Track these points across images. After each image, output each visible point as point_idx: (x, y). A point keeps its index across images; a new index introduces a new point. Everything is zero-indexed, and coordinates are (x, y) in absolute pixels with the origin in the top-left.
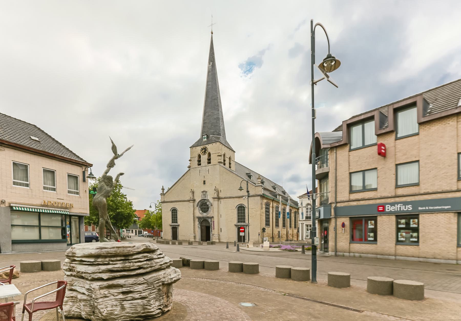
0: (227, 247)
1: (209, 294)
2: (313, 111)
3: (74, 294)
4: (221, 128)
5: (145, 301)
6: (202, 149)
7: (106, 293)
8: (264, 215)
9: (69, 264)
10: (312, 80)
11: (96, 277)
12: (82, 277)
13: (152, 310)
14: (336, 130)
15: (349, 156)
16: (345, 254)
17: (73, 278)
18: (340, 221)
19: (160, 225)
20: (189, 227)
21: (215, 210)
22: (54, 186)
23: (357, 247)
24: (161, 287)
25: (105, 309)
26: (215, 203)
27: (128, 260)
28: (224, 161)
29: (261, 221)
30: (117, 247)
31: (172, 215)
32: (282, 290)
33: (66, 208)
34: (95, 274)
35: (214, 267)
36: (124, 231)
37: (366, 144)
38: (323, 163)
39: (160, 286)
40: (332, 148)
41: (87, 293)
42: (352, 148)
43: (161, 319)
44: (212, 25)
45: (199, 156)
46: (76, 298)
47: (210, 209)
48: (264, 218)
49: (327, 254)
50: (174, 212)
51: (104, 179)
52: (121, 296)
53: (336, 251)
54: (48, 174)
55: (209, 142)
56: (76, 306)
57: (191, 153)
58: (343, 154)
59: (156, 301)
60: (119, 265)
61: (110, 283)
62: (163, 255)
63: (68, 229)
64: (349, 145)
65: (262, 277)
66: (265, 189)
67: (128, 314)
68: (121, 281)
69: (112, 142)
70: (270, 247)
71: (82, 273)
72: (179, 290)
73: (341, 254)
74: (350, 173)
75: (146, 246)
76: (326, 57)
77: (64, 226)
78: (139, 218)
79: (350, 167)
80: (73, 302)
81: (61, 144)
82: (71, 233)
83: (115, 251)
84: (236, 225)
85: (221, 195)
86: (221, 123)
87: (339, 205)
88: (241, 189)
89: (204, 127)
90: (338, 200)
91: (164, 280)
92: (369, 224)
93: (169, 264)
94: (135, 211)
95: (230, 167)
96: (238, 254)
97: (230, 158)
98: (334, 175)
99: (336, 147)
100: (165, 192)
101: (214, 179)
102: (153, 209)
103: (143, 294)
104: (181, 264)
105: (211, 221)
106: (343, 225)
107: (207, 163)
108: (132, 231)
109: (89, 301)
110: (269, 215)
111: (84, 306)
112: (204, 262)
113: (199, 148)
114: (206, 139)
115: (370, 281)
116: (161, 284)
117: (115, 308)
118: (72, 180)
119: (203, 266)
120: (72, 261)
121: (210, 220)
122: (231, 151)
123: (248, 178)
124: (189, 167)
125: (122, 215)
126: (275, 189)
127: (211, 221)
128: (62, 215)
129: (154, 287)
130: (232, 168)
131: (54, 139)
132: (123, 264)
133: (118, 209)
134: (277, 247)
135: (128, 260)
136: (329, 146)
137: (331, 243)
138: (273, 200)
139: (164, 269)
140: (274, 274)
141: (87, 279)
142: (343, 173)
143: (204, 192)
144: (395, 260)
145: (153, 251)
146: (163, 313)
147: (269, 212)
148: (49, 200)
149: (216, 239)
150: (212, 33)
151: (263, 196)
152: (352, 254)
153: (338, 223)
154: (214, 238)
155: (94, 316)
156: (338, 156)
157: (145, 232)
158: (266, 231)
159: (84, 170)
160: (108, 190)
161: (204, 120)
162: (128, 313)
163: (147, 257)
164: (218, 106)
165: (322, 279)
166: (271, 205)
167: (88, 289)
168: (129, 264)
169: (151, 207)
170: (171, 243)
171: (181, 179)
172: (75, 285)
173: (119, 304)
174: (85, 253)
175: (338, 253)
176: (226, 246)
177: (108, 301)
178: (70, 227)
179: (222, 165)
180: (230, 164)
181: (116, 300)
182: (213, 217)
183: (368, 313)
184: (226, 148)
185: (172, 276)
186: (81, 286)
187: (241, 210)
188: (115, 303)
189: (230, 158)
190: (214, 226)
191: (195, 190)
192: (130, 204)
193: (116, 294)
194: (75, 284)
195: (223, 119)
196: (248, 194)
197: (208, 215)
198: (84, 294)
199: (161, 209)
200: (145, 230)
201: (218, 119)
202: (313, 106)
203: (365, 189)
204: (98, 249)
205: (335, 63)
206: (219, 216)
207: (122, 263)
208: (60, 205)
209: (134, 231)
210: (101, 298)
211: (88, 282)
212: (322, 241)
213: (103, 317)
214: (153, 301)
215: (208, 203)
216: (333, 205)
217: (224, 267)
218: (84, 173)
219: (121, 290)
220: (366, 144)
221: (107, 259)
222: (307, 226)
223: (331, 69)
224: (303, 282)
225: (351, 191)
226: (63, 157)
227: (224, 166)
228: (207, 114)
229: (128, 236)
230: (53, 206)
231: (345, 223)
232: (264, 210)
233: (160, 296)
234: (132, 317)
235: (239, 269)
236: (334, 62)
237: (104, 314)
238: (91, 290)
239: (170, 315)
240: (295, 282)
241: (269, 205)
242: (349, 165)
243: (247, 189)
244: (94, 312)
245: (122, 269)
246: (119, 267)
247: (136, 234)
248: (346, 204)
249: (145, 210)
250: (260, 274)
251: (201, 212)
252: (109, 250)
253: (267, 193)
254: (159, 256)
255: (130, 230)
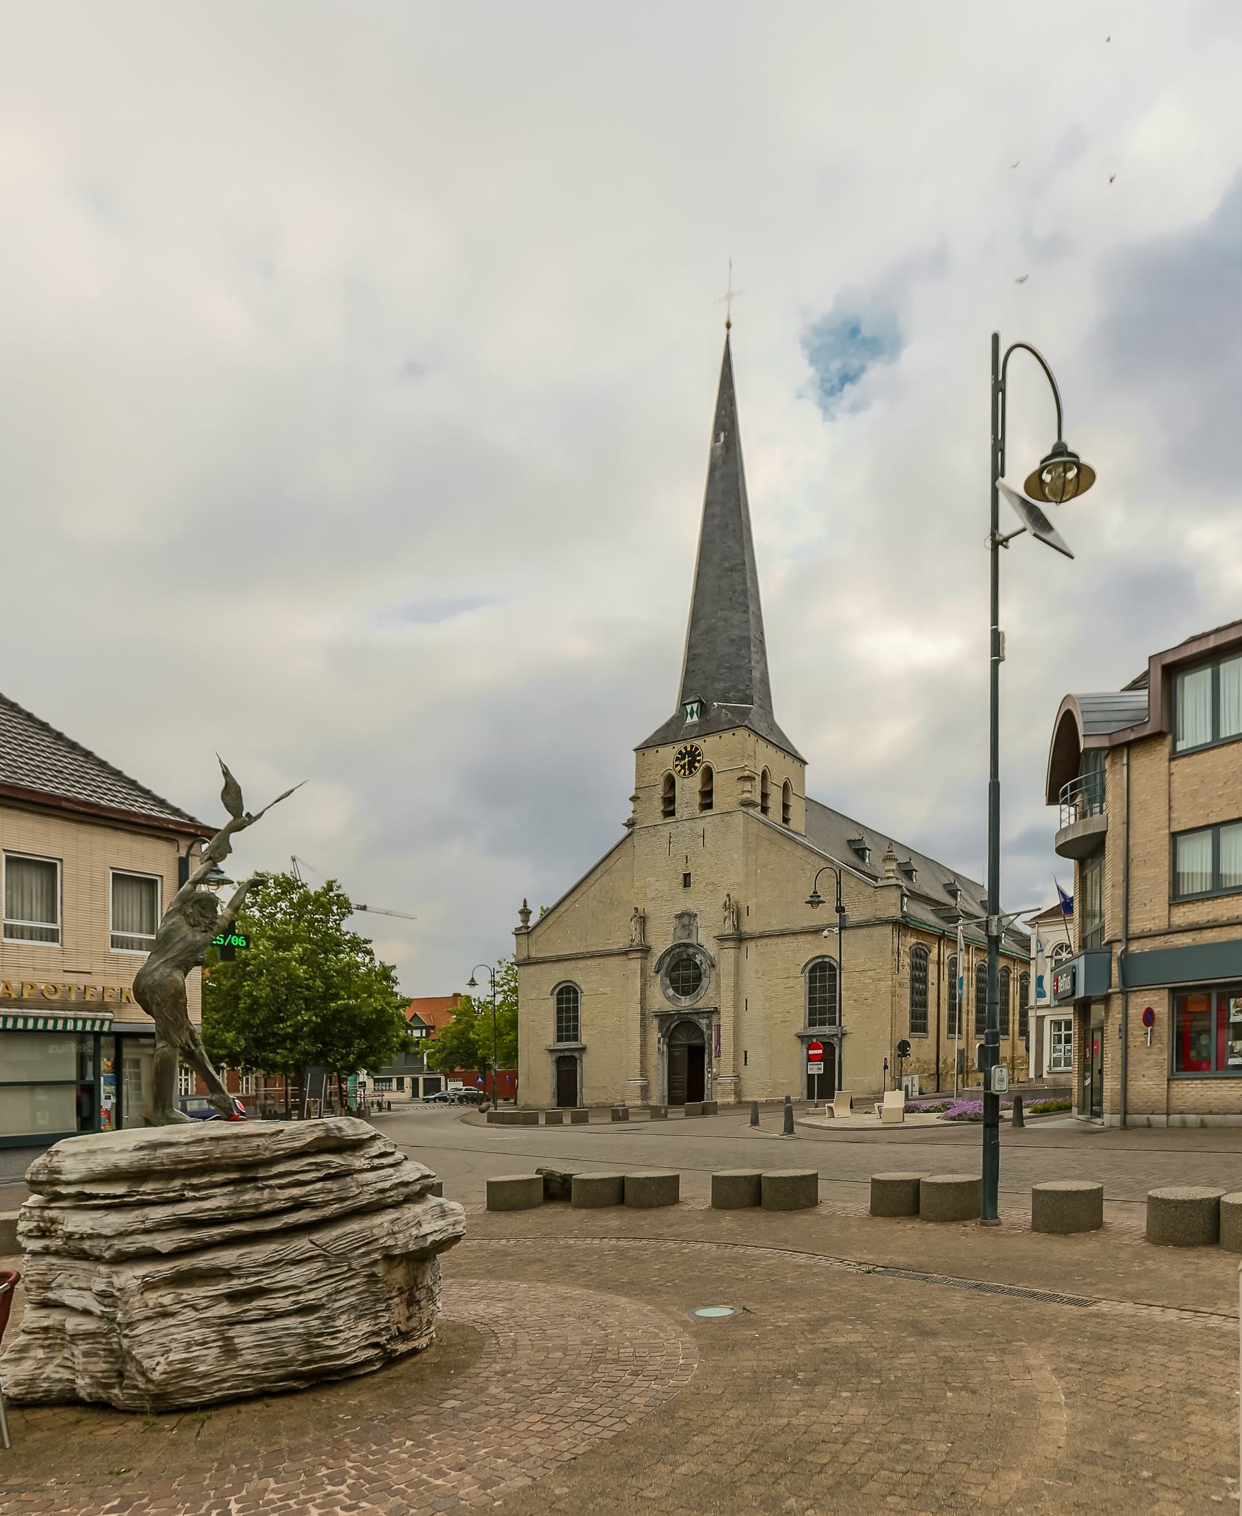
0: (755, 1122)
1: (597, 1288)
2: (997, 639)
3: (54, 1318)
4: (756, 674)
5: (313, 1322)
6: (682, 756)
7: (167, 1300)
8: (907, 992)
9: (37, 1212)
10: (993, 534)
11: (132, 1248)
12: (83, 1251)
13: (341, 1350)
14: (1134, 686)
15: (1171, 774)
16: (1155, 1118)
17: (54, 1260)
18: (1140, 1002)
19: (511, 1055)
20: (622, 1054)
21: (727, 982)
22: (54, 921)
23: (1198, 1092)
24: (379, 1270)
25: (162, 1359)
26: (726, 958)
27: (255, 1179)
28: (765, 796)
29: (893, 1015)
30: (211, 1139)
31: (559, 1011)
32: (869, 1257)
33: (103, 1007)
34: (129, 1239)
35: (662, 1193)
36: (363, 1084)
37: (1225, 733)
38: (1091, 802)
39: (375, 1263)
40: (1115, 750)
41: (97, 1309)
42: (1181, 746)
43: (376, 1380)
44: (729, 296)
45: (670, 782)
46: (61, 1329)
47: (705, 981)
48: (907, 1004)
49: (1097, 1123)
50: (567, 997)
51: (184, 903)
52: (224, 1309)
53: (1125, 1109)
54: (26, 877)
55: (708, 727)
56: (56, 1362)
57: (640, 771)
58: (1149, 768)
59: (359, 1317)
60: (219, 1201)
61: (185, 1264)
62: (399, 1155)
63: (105, 1089)
64: (1170, 738)
65: (824, 1217)
66: (916, 897)
67: (247, 1372)
68: (227, 1258)
69: (226, 773)
70: (908, 1110)
71: (82, 1238)
72: (492, 1284)
73: (1142, 1118)
74: (1174, 836)
75: (328, 1130)
76: (1049, 452)
77: (90, 1077)
78: (428, 1028)
79: (1173, 815)
80: (49, 1346)
81: (88, 754)
82: (118, 1106)
83: (204, 1153)
84: (801, 1037)
85: (750, 925)
86: (754, 657)
87: (1135, 947)
88: (815, 901)
89: (688, 673)
90: (1135, 928)
91: (391, 1242)
92: (1233, 1011)
93: (417, 1187)
94: (407, 1003)
95: (786, 820)
96: (790, 1146)
97: (786, 787)
98: (1121, 842)
99: (1130, 745)
100: (531, 924)
101: (725, 863)
102: (482, 993)
103: (309, 1297)
104: (540, 1193)
105: (709, 1026)
106: (1149, 1017)
107: (661, 815)
108: (400, 1083)
109: (104, 1335)
110: (925, 993)
111: (86, 1354)
112: (623, 1179)
113: (668, 754)
114: (695, 718)
115: (1155, 1204)
116: (377, 1256)
117: (197, 1351)
118: (133, 896)
119: (619, 1194)
120: (51, 1200)
121: (704, 1022)
122: (789, 759)
123: (853, 859)
124: (630, 824)
125: (351, 1020)
126: (953, 893)
127: (709, 1026)
128: (81, 1036)
129: (350, 1269)
130: (793, 824)
131: (59, 736)
132: (234, 1198)
133: (336, 997)
134: (937, 1110)
135: (255, 1179)
136: (1105, 743)
137: (1111, 1085)
138: (941, 937)
139: (396, 1205)
140: (864, 1204)
141: (99, 1259)
142: (1150, 837)
143: (686, 919)
144: (1203, 1125)
145: (356, 1145)
146: (390, 1360)
147: (924, 981)
148: (30, 980)
149: (725, 1094)
150: (728, 326)
151: (903, 925)
152: (1175, 1118)
153: (1131, 1011)
154: (719, 1088)
155: (122, 1389)
156: (1133, 776)
157: (451, 1085)
158: (912, 1050)
159: (183, 853)
160: (194, 944)
161: (690, 647)
162: (248, 1366)
163: (327, 1165)
164: (744, 592)
165: (1015, 1209)
166: (933, 955)
167: (102, 1295)
168: (257, 1195)
169: (472, 983)
170: (542, 1121)
171: (599, 872)
172: (60, 1286)
173: (214, 1336)
174: (92, 1166)
175: (1133, 1118)
176: (782, 1121)
177: (172, 1330)
178: (118, 1082)
179: (756, 812)
180: (786, 807)
181: (204, 1323)
182: (716, 1011)
183: (1104, 1307)
184: (772, 750)
185: (426, 1229)
186: (79, 1288)
187: (822, 979)
188: (198, 1334)
189: (786, 787)
190: (719, 1043)
191: (649, 908)
192: (386, 974)
193: (204, 1303)
194: (59, 1280)
195: (762, 642)
196: (842, 918)
197: (700, 1005)
198: (87, 1313)
199: (515, 990)
200: (451, 1076)
201: (745, 642)
202: (995, 621)
203: (1219, 889)
204: (141, 1148)
205: (1077, 475)
206: (740, 1003)
207: (232, 1193)
208: (73, 998)
209: (408, 1081)
210: (148, 1318)
211: (103, 1269)
212: (1085, 1079)
213: (151, 1387)
214: (344, 1317)
215: (698, 959)
216: (1118, 949)
217: (696, 1193)
218: (183, 864)
219: (223, 1287)
220: (1225, 733)
221: (177, 1183)
222: (1057, 1024)
223: (1063, 494)
224: (953, 1227)
225: (1177, 899)
226: (98, 806)
227: (762, 816)
228: (703, 625)
229: (379, 1104)
230: (47, 1004)
231: (1156, 1010)
232: (906, 973)
233: (378, 1301)
234: (265, 1380)
235: (748, 1195)
236: (1075, 470)
237: (156, 1376)
238: (112, 1296)
239: (414, 1364)
240: (930, 1226)
241: (925, 957)
242: (1170, 808)
243: (839, 899)
244: (121, 1375)
245: (229, 1213)
246: (218, 1208)
247: (415, 1094)
248: (1158, 943)
249: (456, 995)
250: (822, 1210)
251: (671, 992)
252: (183, 1149)
253: (923, 913)
254: (377, 1162)
255: (390, 1080)
